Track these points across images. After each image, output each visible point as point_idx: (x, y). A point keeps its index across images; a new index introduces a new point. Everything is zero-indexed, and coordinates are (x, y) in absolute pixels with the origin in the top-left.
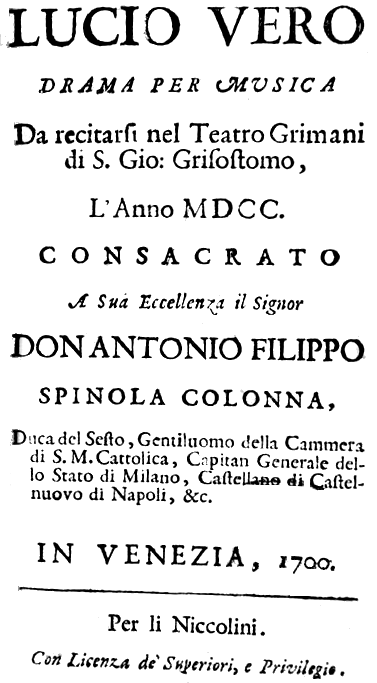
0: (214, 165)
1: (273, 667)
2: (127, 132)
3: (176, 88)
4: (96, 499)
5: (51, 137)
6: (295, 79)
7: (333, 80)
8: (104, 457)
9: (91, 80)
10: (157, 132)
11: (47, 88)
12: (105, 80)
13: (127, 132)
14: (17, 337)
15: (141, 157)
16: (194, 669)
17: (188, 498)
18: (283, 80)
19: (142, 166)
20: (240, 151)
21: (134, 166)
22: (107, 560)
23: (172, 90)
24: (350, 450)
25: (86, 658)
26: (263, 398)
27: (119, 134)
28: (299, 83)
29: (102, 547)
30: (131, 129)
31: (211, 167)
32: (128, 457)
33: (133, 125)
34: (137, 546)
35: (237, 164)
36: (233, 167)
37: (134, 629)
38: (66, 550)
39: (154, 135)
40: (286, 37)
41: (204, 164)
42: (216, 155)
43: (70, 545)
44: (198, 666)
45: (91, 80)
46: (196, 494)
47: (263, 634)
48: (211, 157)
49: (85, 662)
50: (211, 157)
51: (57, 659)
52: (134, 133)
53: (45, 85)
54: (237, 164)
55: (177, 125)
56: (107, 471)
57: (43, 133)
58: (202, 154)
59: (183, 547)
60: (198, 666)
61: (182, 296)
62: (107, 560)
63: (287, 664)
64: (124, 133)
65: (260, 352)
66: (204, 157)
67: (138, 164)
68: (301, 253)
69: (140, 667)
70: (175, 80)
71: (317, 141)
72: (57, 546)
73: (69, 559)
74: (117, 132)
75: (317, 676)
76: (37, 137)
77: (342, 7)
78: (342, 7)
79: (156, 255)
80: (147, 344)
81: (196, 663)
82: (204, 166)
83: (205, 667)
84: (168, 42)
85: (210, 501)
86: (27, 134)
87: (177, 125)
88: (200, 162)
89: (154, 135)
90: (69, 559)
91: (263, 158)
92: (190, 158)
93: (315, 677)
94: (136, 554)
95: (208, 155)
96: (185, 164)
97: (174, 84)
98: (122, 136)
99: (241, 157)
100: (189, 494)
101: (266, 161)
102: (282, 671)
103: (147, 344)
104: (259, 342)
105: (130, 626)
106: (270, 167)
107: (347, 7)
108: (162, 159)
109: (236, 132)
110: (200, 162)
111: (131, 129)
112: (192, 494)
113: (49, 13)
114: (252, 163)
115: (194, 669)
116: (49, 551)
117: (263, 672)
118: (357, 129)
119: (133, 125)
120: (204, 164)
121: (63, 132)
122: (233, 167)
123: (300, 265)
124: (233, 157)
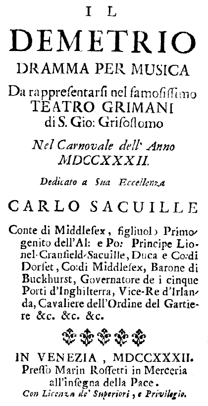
1: (152, 394)
2: (102, 91)
13: (102, 91)
15: (84, 121)
16: (109, 396)
17: (65, 317)
24: (107, 282)
25: (51, 392)
27: (98, 92)
30: (104, 89)
32: (41, 290)
33: (106, 87)
38: (26, 355)
39: (114, 93)
40: (56, 360)
41: (117, 125)
43: (28, 354)
44: (111, 395)
46: (69, 314)
49: (50, 395)
51: (37, 394)
52: (106, 91)
58: (115, 119)
60: (111, 395)
61: (144, 180)
63: (158, 392)
64: (101, 92)
69: (83, 184)
71: (150, 127)
74: (96, 91)
75: (174, 398)
76: (20, 92)
77: (185, 32)
78: (185, 32)
79: (101, 206)
81: (110, 393)
83: (115, 395)
84: (186, 52)
85: (78, 318)
86: (14, 91)
88: (114, 124)
89: (114, 93)
93: (173, 399)
94: (111, 68)
98: (99, 94)
100: (65, 314)
102: (156, 396)
104: (45, 33)
106: (184, 235)
107: (187, 33)
112: (67, 314)
113: (164, 97)
115: (109, 396)
117: (147, 396)
118: (125, 368)
119: (106, 87)
120: (117, 125)
121: (59, 91)
123: (68, 111)
124: (106, 370)
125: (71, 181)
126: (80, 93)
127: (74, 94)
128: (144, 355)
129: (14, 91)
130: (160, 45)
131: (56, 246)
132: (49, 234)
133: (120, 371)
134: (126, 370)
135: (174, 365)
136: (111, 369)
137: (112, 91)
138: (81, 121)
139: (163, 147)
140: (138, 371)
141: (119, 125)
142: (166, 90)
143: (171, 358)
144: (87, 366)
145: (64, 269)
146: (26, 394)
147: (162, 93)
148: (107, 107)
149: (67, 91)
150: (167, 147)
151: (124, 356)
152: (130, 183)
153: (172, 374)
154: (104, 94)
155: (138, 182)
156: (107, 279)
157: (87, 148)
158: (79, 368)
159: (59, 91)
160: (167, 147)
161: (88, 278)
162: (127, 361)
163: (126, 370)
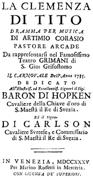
0: (35, 67)
3: (50, 32)
4: (59, 140)
5: (11, 55)
6: (74, 30)
7: (83, 31)
8: (58, 132)
9: (24, 30)
10: (52, 54)
11: (12, 32)
12: (27, 30)
14: (71, 45)
15: (35, 66)
18: (71, 30)
19: (35, 68)
20: (59, 65)
21: (33, 68)
22: (17, 162)
23: (49, 32)
26: (68, 139)
27: (34, 37)
28: (75, 31)
29: (15, 160)
30: (76, 53)
31: (53, 68)
32: (52, 167)
33: (46, 52)
34: (43, 3)
35: (59, 68)
36: (58, 68)
37: (16, 168)
38: (8, 160)
39: (51, 55)
42: (54, 65)
43: (30, 160)
45: (24, 30)
47: (80, 139)
48: (53, 66)
50: (53, 66)
52: (46, 54)
53: (12, 31)
54: (59, 68)
55: (56, 53)
56: (59, 136)
57: (10, 54)
58: (51, 65)
59: (43, 3)
62: (17, 162)
65: (61, 55)
66: (51, 66)
67: (34, 67)
68: (21, 59)
70: (50, 30)
72: (7, 160)
73: (9, 162)
76: (8, 55)
80: (40, 18)
82: (51, 68)
84: (73, 17)
86: (6, 54)
87: (56, 53)
88: (50, 67)
90: (9, 162)
91: (65, 66)
92: (48, 66)
95: (52, 65)
96: (32, 67)
97: (49, 31)
99: (59, 66)
101: (65, 67)
103: (40, 18)
105: (15, 168)
108: (39, 66)
109: (37, 54)
110: (50, 67)
111: (46, 53)
114: (62, 67)
116: (5, 161)
118: (53, 166)
119: (46, 52)
121: (25, 54)
122: (65, 68)
124: (58, 66)
125: (53, 90)
126: (35, 55)
127: (32, 55)
128: (70, 161)
129: (6, 54)
130: (14, 18)
131: (54, 111)
132: (85, 105)
133: (51, 168)
134: (54, 167)
135: (77, 165)
136: (48, 167)
137: (50, 54)
138: (33, 66)
139: (68, 76)
140: (60, 168)
141: (52, 67)
142: (77, 53)
143: (78, 162)
144: (36, 165)
145: (25, 126)
146: (15, 174)
147: (75, 55)
148: (41, 61)
149: (29, 54)
150: (69, 76)
151: (62, 161)
152: (42, 89)
153: (76, 169)
154: (45, 55)
155: (45, 89)
156: (25, 132)
157: (32, 75)
158: (30, 167)
159: (25, 54)
160: (69, 76)
161: (33, 66)
162: (63, 163)
163: (54, 167)
